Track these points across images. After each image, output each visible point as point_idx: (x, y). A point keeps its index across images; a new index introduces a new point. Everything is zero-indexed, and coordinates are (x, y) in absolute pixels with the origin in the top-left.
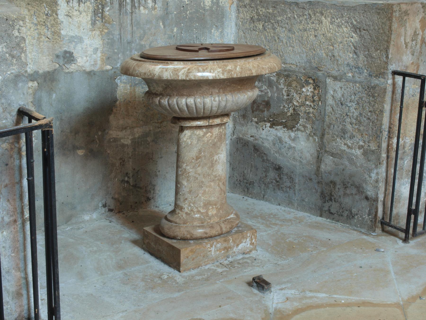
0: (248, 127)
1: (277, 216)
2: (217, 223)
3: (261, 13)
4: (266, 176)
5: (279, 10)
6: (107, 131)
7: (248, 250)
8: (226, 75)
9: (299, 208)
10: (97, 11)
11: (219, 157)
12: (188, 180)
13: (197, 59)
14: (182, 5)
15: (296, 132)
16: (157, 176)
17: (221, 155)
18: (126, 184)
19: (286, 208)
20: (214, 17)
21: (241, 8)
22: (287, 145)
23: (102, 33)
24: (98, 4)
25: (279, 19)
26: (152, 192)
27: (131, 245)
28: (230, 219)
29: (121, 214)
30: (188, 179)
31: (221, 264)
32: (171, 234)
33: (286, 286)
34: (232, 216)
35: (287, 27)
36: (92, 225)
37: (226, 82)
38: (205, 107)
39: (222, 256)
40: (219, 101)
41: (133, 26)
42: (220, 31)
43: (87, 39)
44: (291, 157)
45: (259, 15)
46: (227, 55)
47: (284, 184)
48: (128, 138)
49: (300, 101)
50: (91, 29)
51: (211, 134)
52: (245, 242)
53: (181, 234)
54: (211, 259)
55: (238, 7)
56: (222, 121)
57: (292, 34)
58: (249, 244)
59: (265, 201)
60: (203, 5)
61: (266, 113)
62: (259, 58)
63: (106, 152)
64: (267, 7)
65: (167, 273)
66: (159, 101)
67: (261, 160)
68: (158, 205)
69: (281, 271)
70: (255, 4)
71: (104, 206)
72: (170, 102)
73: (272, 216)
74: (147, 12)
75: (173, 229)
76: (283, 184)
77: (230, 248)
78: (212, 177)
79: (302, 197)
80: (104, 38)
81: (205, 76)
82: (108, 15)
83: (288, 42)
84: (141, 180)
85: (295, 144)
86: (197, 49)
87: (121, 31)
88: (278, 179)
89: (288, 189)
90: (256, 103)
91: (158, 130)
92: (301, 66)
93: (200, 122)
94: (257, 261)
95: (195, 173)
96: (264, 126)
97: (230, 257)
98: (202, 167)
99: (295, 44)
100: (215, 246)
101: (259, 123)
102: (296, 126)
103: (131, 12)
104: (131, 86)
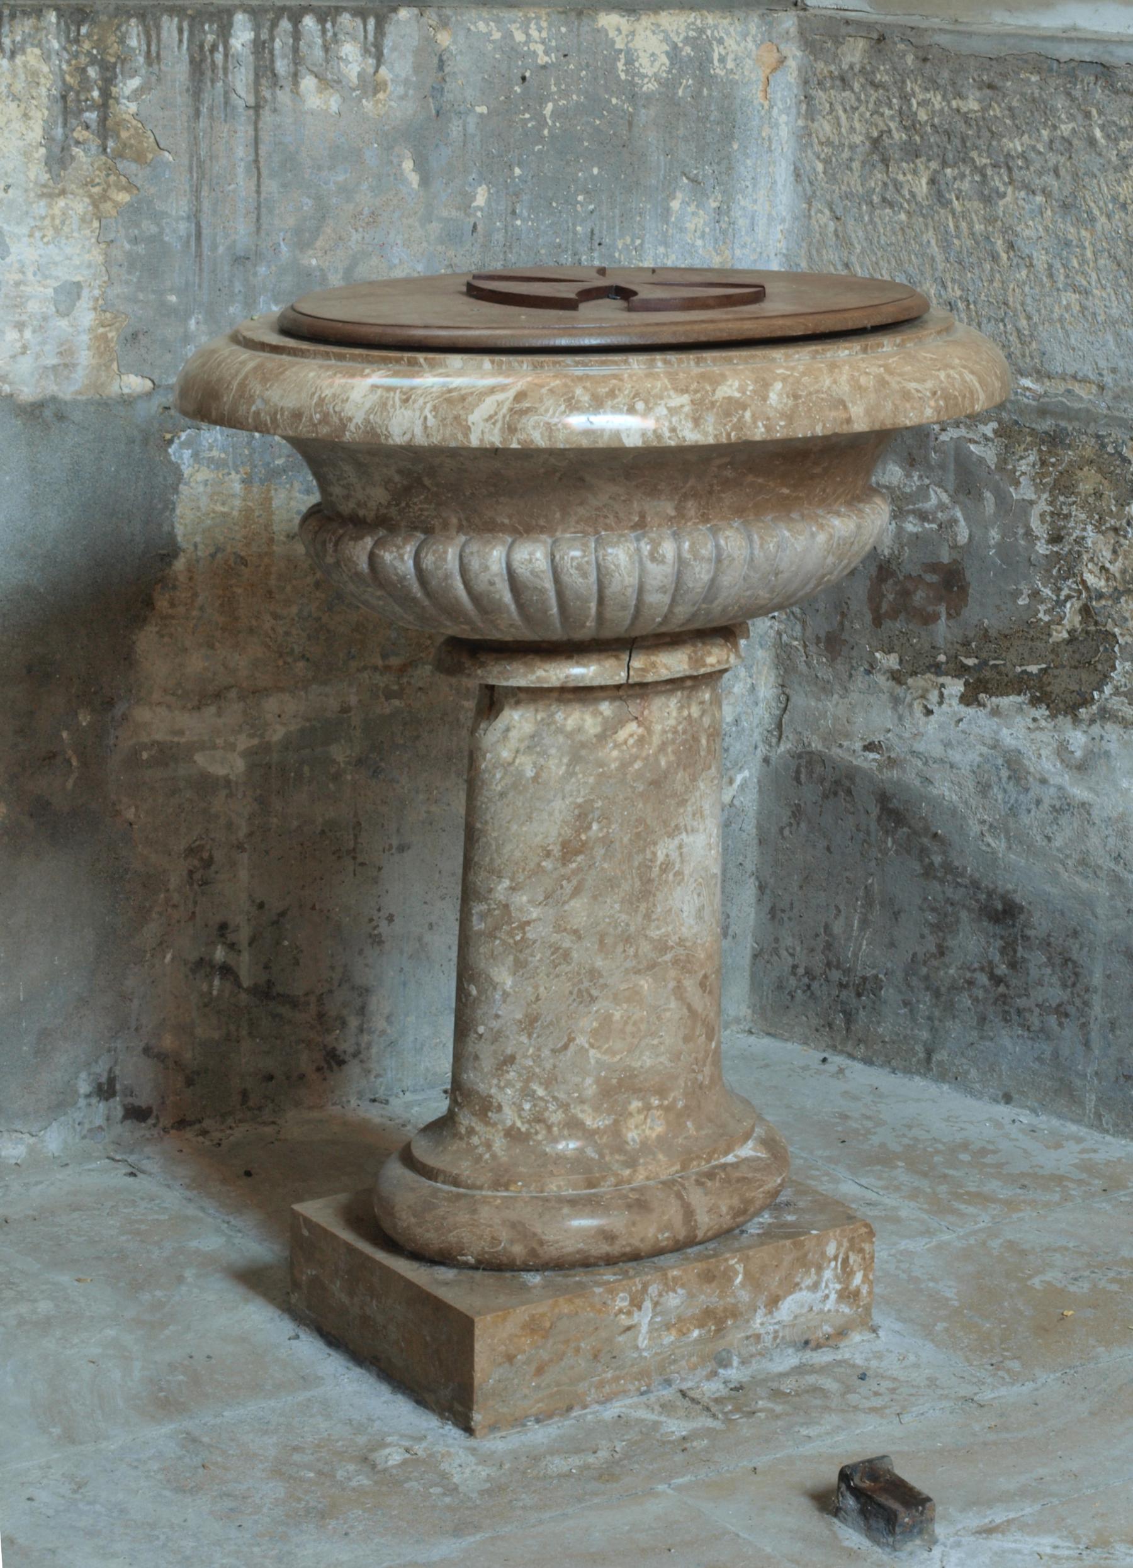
0: (855, 697)
1: (989, 1159)
2: (668, 1184)
3: (923, 116)
4: (941, 951)
5: (1015, 104)
6: (120, 709)
7: (828, 1329)
8: (710, 429)
9: (1108, 1118)
10: (78, 93)
11: (680, 847)
12: (519, 965)
13: (563, 342)
14: (517, 73)
15: (1096, 729)
16: (381, 942)
17: (691, 839)
18: (216, 982)
19: (1044, 1118)
20: (681, 132)
21: (824, 90)
22: (1049, 796)
23: (101, 206)
24: (83, 60)
25: (1016, 145)
26: (353, 1022)
27: (233, 1293)
28: (735, 1166)
29: (189, 1134)
30: (522, 957)
31: (683, 1394)
32: (429, 1236)
33: (1012, 1515)
34: (747, 1150)
35: (1055, 190)
36: (40, 1187)
37: (718, 462)
38: (608, 592)
39: (691, 1355)
40: (680, 560)
41: (265, 172)
42: (714, 205)
43: (25, 239)
44: (1067, 856)
45: (911, 125)
46: (722, 325)
47: (1033, 993)
48: (232, 747)
49: (1114, 569)
50: (44, 186)
51: (641, 731)
52: (815, 1287)
53: (481, 1237)
54: (635, 1369)
55: (806, 82)
56: (697, 662)
57: (1078, 222)
58: (833, 1296)
59: (936, 1081)
60: (627, 72)
61: (943, 630)
62: (888, 344)
63: (118, 813)
64: (954, 84)
65: (402, 1436)
66: (372, 557)
67: (918, 868)
68: (381, 1094)
69: (991, 1437)
70: (895, 69)
71: (105, 1090)
72: (428, 561)
73: (965, 1157)
74: (334, 103)
75: (441, 1212)
76: (1028, 996)
77: (734, 1312)
78: (645, 947)
79: (1120, 1061)
80: (112, 236)
81: (603, 431)
82: (135, 116)
83: (1057, 264)
84: (297, 963)
85: (1090, 789)
86: (573, 296)
87: (198, 198)
88: (1002, 969)
89: (1053, 1020)
90: (893, 574)
91: (386, 708)
92: (1124, 390)
93: (584, 666)
94: (871, 1384)
95: (558, 929)
96: (934, 696)
97: (735, 1361)
98: (595, 898)
99: (1094, 276)
100: (656, 1304)
101: (910, 681)
102: (1096, 694)
103: (251, 101)
104: (247, 482)
